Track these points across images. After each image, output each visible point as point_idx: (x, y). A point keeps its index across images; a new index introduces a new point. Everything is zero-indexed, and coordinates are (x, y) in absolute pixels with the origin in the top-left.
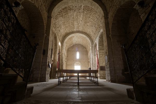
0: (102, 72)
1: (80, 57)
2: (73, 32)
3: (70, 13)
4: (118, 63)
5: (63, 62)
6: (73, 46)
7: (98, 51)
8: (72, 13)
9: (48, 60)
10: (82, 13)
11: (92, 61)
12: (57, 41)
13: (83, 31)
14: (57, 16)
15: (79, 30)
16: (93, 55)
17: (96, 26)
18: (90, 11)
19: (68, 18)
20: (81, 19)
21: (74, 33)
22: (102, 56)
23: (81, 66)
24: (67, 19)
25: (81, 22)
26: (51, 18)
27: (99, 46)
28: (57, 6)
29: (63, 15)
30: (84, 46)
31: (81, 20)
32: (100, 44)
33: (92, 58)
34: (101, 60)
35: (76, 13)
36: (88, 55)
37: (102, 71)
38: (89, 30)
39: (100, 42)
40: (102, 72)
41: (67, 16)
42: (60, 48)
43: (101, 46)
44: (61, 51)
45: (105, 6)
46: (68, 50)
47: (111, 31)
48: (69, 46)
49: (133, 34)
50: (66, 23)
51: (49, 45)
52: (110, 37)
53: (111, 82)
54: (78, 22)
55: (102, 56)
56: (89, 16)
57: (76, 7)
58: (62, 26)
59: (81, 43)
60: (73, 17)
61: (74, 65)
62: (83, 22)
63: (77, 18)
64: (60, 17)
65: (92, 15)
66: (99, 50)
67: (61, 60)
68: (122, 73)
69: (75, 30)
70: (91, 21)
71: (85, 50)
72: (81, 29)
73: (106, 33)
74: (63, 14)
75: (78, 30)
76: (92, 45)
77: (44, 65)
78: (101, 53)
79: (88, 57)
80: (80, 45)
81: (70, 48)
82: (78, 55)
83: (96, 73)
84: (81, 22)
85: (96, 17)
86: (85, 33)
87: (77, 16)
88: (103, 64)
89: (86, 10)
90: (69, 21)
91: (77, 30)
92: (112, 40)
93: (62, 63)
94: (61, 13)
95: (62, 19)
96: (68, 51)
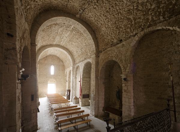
0: (84, 100)
1: (55, 73)
2: (51, 46)
6: (46, 57)
7: (81, 79)
8: (56, 28)
10: (70, 32)
11: (73, 85)
13: (65, 46)
16: (74, 77)
17: (83, 50)
19: (50, 33)
22: (85, 84)
23: (57, 84)
26: (35, 46)
27: (83, 73)
31: (66, 37)
33: (73, 81)
36: (66, 72)
38: (72, 49)
40: (84, 100)
41: (50, 30)
45: (98, 41)
47: (99, 73)
53: (95, 117)
55: (85, 84)
59: (58, 55)
60: (57, 31)
61: (47, 83)
66: (83, 78)
69: (55, 43)
70: (78, 43)
72: (62, 44)
75: (59, 44)
77: (34, 113)
79: (65, 73)
91: (58, 43)
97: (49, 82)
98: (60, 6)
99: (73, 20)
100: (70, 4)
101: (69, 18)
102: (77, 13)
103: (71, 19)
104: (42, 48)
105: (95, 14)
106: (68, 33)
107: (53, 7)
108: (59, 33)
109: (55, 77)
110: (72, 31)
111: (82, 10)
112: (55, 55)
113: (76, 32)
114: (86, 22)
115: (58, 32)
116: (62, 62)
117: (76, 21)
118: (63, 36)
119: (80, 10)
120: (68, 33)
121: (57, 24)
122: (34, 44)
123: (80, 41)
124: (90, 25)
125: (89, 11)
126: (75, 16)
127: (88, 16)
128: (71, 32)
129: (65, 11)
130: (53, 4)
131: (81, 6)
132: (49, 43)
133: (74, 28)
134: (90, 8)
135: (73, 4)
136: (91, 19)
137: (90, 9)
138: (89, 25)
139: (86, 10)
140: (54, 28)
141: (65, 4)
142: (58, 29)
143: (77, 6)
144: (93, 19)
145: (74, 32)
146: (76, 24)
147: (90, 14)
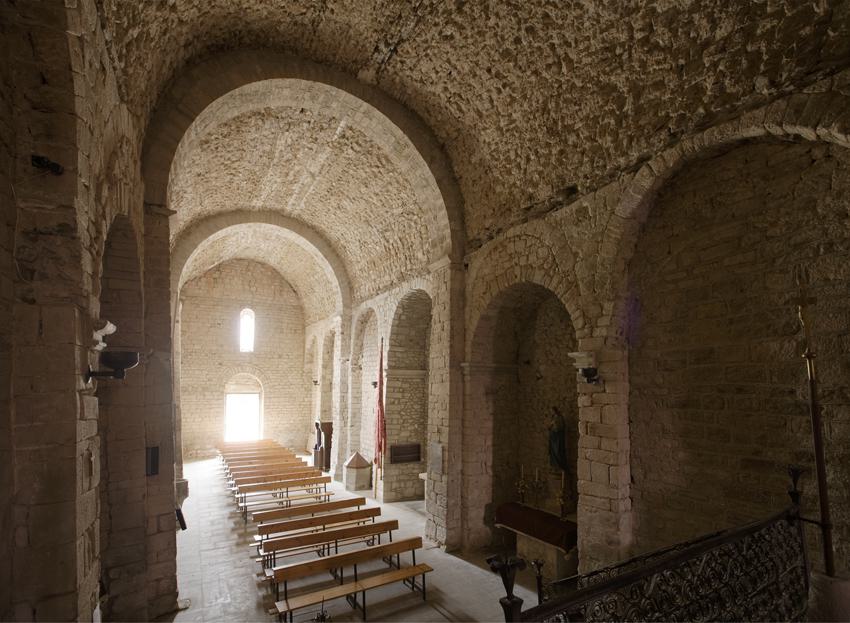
0: (396, 472)
1: (258, 343)
2: (240, 215)
3: (257, 129)
4: (477, 482)
6: (218, 268)
7: (384, 374)
8: (266, 133)
10: (329, 149)
13: (306, 217)
15: (283, 210)
17: (393, 237)
18: (379, 159)
19: (238, 154)
21: (247, 221)
25: (305, 179)
26: (166, 217)
27: (391, 345)
30: (283, 278)
32: (397, 334)
33: (344, 383)
34: (393, 416)
36: (309, 338)
37: (394, 466)
39: (397, 326)
40: (396, 472)
43: (400, 349)
45: (460, 194)
49: (538, 379)
50: (214, 175)
52: (462, 368)
53: (449, 551)
54: (287, 174)
56: (364, 175)
58: (190, 189)
59: (272, 261)
60: (267, 148)
62: (320, 182)
65: (380, 183)
66: (390, 367)
68: (485, 519)
69: (258, 203)
71: (293, 301)
72: (293, 206)
73: (451, 346)
76: (346, 306)
77: (159, 531)
78: (399, 384)
79: (308, 346)
80: (263, 264)
82: (247, 329)
85: (404, 204)
86: (313, 228)
88: (403, 434)
91: (272, 204)
92: (468, 385)
97: (230, 387)
98: (282, 28)
99: (343, 95)
100: (329, 20)
102: (365, 64)
104: (197, 225)
105: (447, 66)
106: (322, 158)
108: (277, 155)
109: (260, 361)
110: (339, 147)
117: (360, 101)
118: (297, 168)
119: (377, 49)
120: (322, 158)
121: (269, 114)
122: (160, 206)
127: (416, 75)
131: (383, 30)
132: (229, 205)
133: (349, 133)
135: (342, 18)
136: (432, 89)
137: (426, 41)
139: (406, 46)
141: (306, 21)
142: (275, 138)
143: (362, 28)
144: (438, 89)
145: (350, 151)
147: (425, 66)
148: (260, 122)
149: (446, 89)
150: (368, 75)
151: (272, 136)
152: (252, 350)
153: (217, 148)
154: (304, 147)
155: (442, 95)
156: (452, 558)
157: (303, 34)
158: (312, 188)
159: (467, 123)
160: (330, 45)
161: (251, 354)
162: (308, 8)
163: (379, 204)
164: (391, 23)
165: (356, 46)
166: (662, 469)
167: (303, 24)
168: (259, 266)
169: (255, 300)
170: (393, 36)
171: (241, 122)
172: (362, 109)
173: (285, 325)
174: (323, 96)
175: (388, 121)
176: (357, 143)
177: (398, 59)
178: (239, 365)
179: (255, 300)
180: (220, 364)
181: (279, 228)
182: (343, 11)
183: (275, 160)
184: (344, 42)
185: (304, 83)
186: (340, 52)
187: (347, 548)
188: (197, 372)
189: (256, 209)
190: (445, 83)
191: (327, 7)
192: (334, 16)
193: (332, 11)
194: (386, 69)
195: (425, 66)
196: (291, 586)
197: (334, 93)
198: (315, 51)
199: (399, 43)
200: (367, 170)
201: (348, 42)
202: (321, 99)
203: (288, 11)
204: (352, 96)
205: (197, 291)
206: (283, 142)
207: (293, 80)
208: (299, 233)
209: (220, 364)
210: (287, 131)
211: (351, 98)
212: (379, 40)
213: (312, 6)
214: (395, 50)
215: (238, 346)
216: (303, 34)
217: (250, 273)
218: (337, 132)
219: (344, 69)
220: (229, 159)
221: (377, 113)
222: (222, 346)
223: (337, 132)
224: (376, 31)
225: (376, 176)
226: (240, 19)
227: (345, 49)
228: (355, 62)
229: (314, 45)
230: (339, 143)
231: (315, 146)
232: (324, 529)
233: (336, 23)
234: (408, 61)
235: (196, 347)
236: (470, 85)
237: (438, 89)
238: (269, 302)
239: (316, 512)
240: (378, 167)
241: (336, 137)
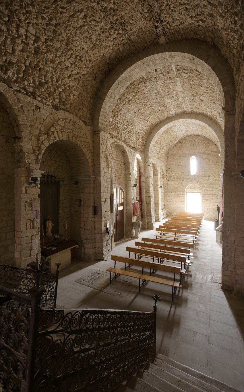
2: (169, 119)
5: (149, 196)
6: (181, 141)
8: (150, 86)
9: (103, 219)
12: (127, 158)
13: (195, 110)
14: (116, 109)
19: (146, 99)
20: (181, 90)
24: (143, 101)
25: (181, 95)
28: (107, 98)
29: (131, 98)
35: (162, 81)
41: (142, 96)
42: (142, 165)
44: (145, 170)
46: (169, 155)
48: (170, 146)
51: (103, 190)
57: (156, 70)
58: (136, 118)
63: (166, 90)
64: (123, 107)
65: (205, 81)
67: (146, 192)
69: (172, 112)
70: (207, 93)
72: (187, 108)
74: (128, 97)
77: (98, 233)
80: (199, 136)
81: (173, 148)
83: (164, 336)
84: (181, 95)
86: (201, 114)
87: (166, 86)
89: (186, 72)
90: (149, 103)
91: (178, 111)
93: (147, 197)
94: (124, 98)
95: (129, 108)
96: (168, 157)
97: (187, 189)
98: (121, 50)
99: (157, 56)
100: (132, 34)
101: (148, 58)
102: (158, 37)
103: (152, 57)
104: (153, 129)
105: (181, 7)
106: (178, 83)
107: (113, 59)
108: (162, 92)
109: (199, 179)
110: (180, 76)
111: (157, 22)
112: (196, 134)
113: (187, 73)
114: (187, 39)
115: (159, 92)
116: (215, 145)
117: (164, 53)
118: (174, 92)
119: (156, 27)
120: (178, 83)
121: (145, 80)
122: (97, 131)
123: (208, 88)
124: (197, 36)
125: (170, 12)
126: (158, 43)
127: (177, 23)
128: (181, 77)
129: (136, 49)
130: (108, 55)
131: (151, 18)
132: (162, 118)
133: (178, 67)
134: (165, 5)
135: (136, 28)
136: (186, 23)
137: (167, 5)
138: (197, 39)
139: (162, 15)
140: (144, 88)
141: (126, 41)
142: (155, 86)
143: (145, 24)
144: (190, 21)
145: (185, 75)
146: (169, 59)
147: (176, 15)
148: (144, 85)
149: (192, 17)
150: (162, 40)
151: (153, 86)
152: (191, 174)
153: (135, 101)
154: (169, 83)
155: (193, 21)
156: (221, 294)
157: (129, 45)
158: (187, 97)
159: (211, 25)
160: (141, 41)
161: (196, 175)
162: (122, 37)
163: (211, 92)
164: (151, 12)
165: (149, 33)
166: (219, 272)
167: (126, 43)
168: (197, 137)
169: (196, 152)
170: (155, 17)
171: (137, 88)
172: (168, 56)
173: (211, 161)
174: (150, 62)
175: (179, 53)
176: (184, 69)
177: (165, 23)
178: (190, 180)
179: (196, 152)
180: (183, 180)
181: (185, 119)
182: (133, 26)
183: (163, 94)
184: (145, 36)
185: (139, 63)
186: (147, 40)
187: (167, 263)
188: (174, 184)
189: (174, 115)
190: (189, 14)
191: (128, 30)
192: (133, 31)
193: (131, 29)
194: (166, 31)
195: (176, 15)
196: (158, 273)
197: (153, 58)
198: (139, 47)
199: (160, 17)
200: (196, 79)
201: (146, 34)
202: (151, 63)
203: (117, 43)
204: (160, 54)
205: (173, 153)
206: (159, 86)
207: (135, 65)
208: (195, 118)
209: (183, 180)
210: (157, 81)
211: (160, 55)
212: (153, 23)
213: (122, 35)
214: (162, 21)
215: (190, 172)
216: (129, 45)
217: (193, 141)
218: (174, 70)
219: (154, 45)
220: (144, 102)
221: (174, 53)
222: (183, 173)
223: (174, 70)
224: (150, 21)
225: (201, 80)
226: (105, 59)
227: (148, 38)
228: (155, 39)
229: (136, 46)
230: (179, 74)
231: (172, 81)
232: (161, 251)
233: (135, 32)
234: (169, 20)
235: (173, 174)
236: (196, 5)
237: (190, 21)
238: (203, 152)
239: (167, 244)
240: (199, 75)
241: (175, 72)
